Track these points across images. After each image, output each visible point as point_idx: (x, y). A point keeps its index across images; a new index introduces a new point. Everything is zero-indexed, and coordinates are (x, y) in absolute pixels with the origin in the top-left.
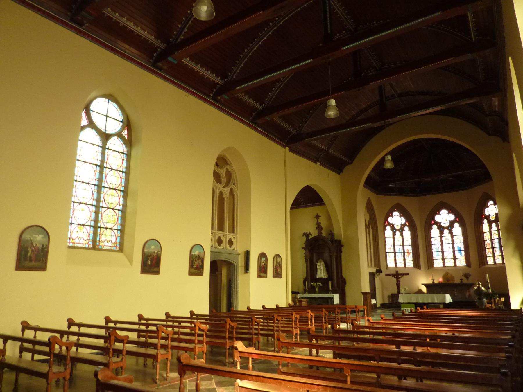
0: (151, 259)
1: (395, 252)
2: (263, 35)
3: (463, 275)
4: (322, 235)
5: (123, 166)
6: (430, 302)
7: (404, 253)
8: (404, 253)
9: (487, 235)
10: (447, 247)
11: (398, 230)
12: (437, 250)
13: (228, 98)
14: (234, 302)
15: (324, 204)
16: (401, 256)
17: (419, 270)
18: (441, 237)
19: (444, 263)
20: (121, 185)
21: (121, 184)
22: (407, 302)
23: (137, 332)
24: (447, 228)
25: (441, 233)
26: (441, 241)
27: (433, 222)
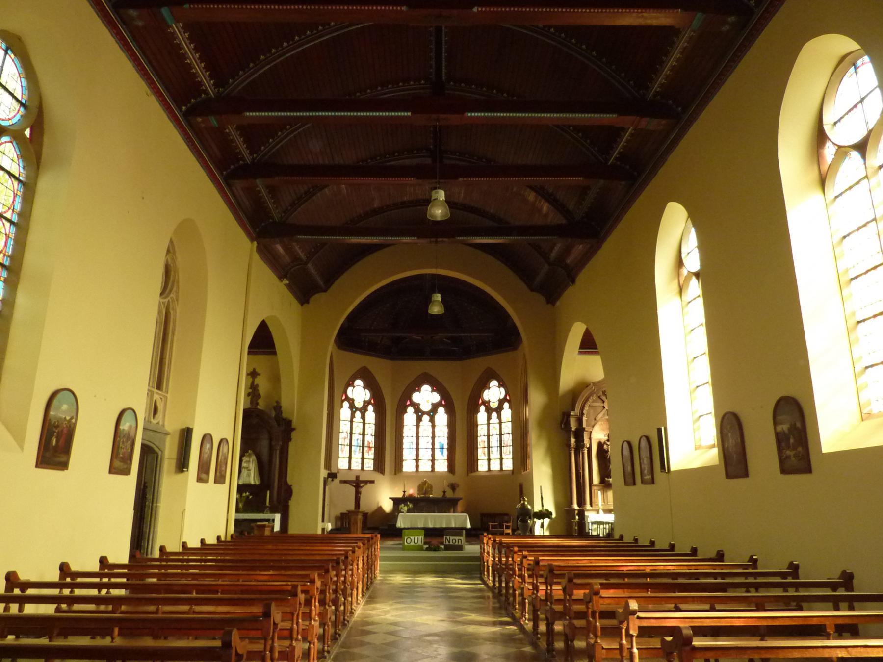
0: (58, 433)
1: (351, 446)
2: (312, 35)
3: (448, 486)
4: (258, 407)
5: (14, 209)
6: (444, 526)
7: (363, 447)
8: (363, 447)
9: (482, 429)
10: (425, 442)
11: (428, 413)
12: (410, 446)
13: (217, 126)
14: (149, 531)
15: (275, 353)
16: (359, 452)
17: (382, 475)
18: (418, 426)
19: (417, 466)
20: (4, 252)
21: (6, 252)
22: (409, 527)
23: (17, 603)
24: (428, 413)
25: (419, 420)
26: (418, 433)
27: (408, 403)
